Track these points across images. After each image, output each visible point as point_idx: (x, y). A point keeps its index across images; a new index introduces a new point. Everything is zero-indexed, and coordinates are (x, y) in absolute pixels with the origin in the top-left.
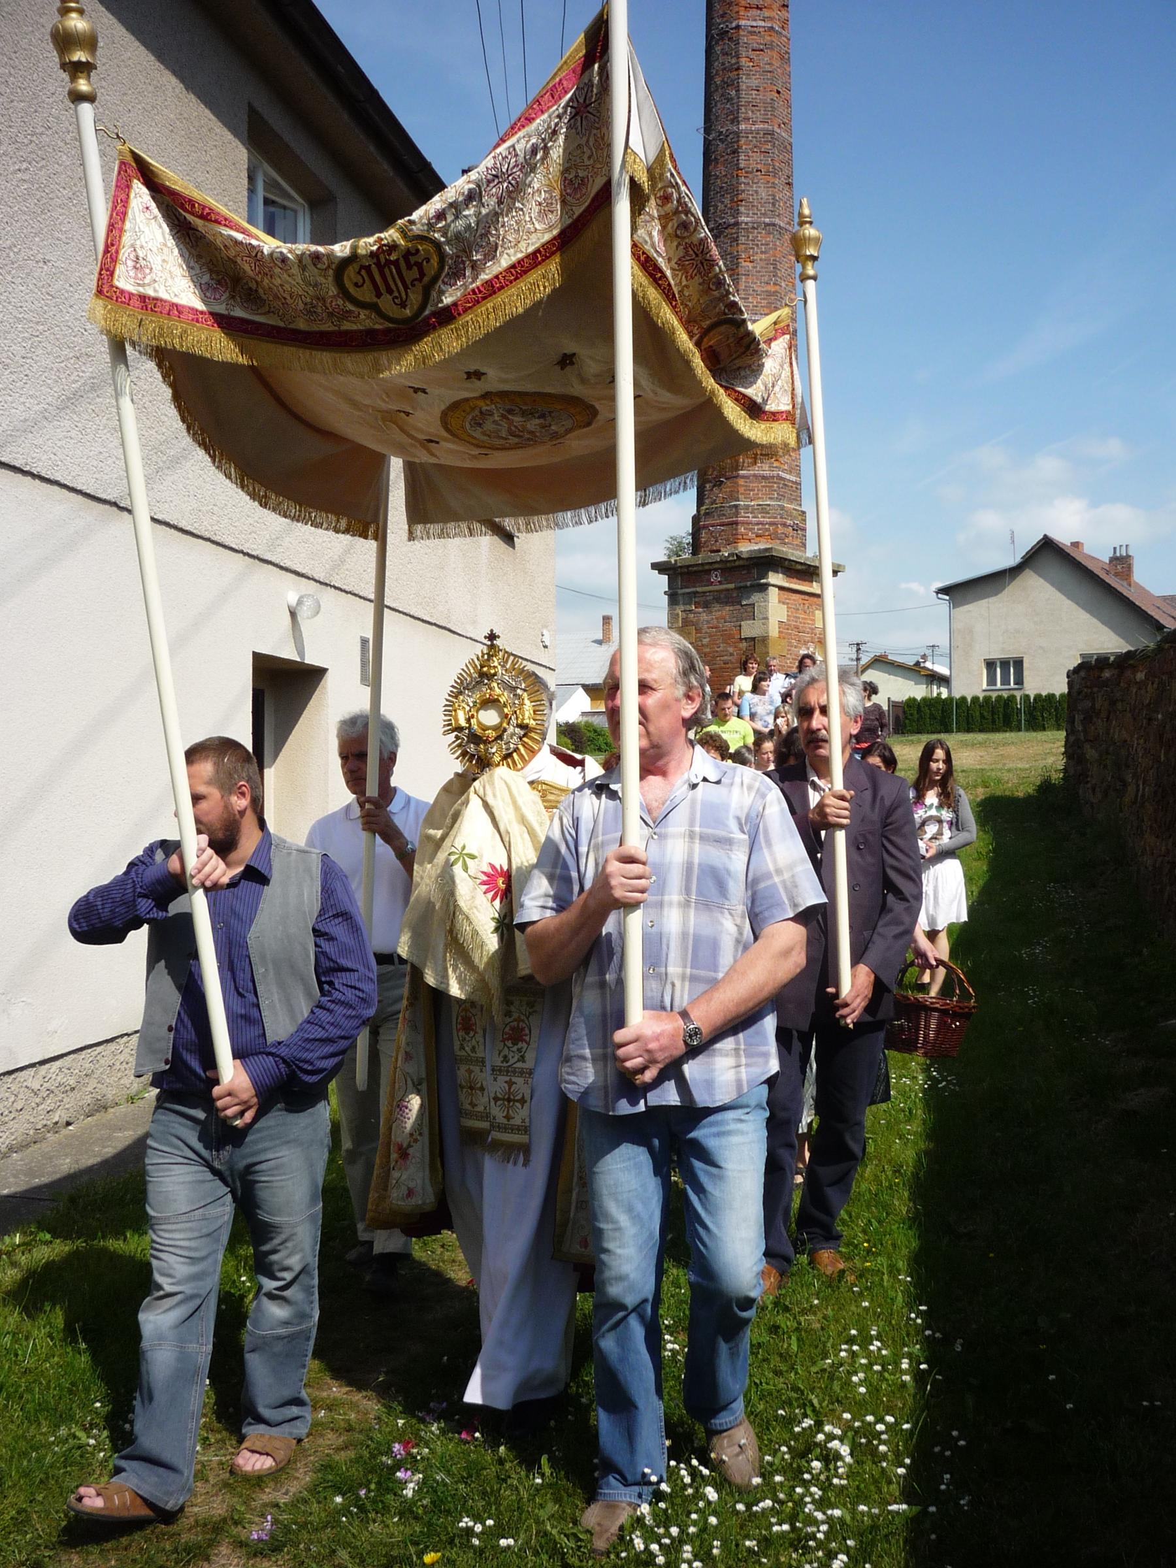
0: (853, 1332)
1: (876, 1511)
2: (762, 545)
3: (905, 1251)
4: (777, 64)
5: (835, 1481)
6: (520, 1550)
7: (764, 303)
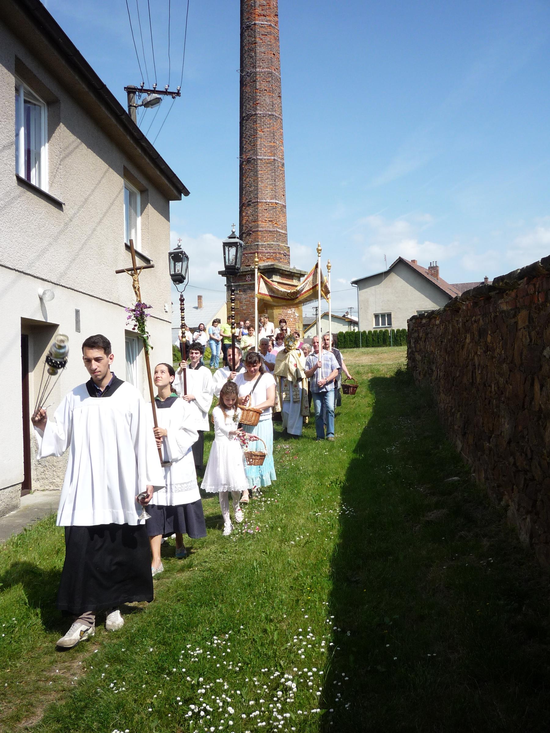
0: (300, 630)
2: (269, 263)
3: (326, 591)
4: (273, 41)
5: (288, 700)
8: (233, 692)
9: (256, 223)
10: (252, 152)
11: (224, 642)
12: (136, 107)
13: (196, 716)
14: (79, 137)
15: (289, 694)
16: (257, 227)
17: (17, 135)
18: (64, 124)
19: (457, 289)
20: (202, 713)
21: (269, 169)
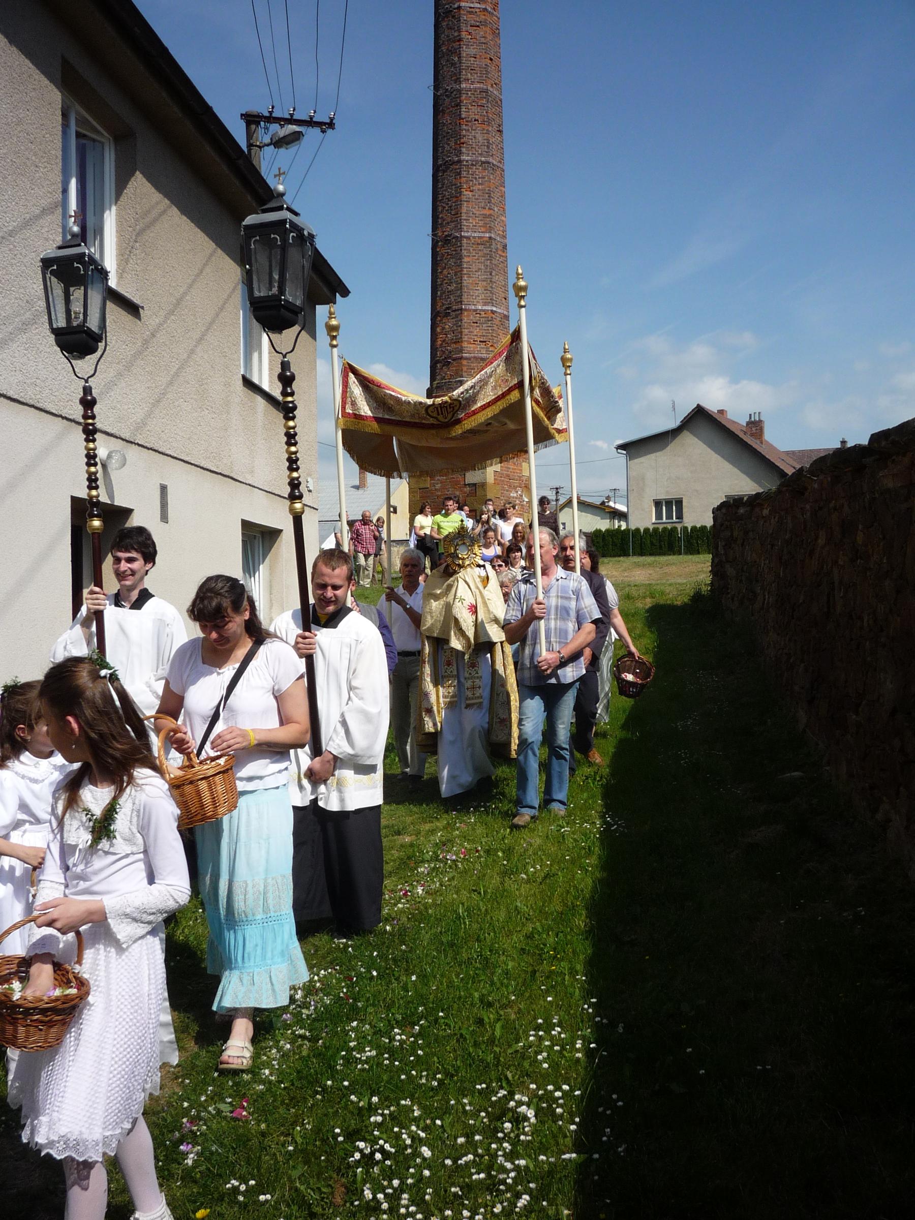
0: (540, 1021)
1: (552, 1160)
3: (582, 957)
4: (490, 37)
5: (522, 1137)
6: (275, 1202)
7: (481, 223)
8: (428, 1122)
9: (457, 346)
10: (453, 225)
11: (412, 1039)
12: (260, 147)
13: (368, 1160)
14: (166, 195)
15: (524, 1128)
16: (461, 351)
17: (65, 191)
18: (142, 173)
19: (795, 460)
20: (378, 1156)
21: (481, 253)
